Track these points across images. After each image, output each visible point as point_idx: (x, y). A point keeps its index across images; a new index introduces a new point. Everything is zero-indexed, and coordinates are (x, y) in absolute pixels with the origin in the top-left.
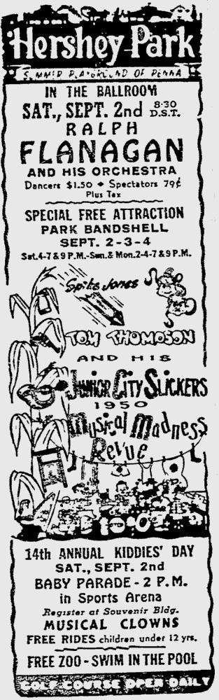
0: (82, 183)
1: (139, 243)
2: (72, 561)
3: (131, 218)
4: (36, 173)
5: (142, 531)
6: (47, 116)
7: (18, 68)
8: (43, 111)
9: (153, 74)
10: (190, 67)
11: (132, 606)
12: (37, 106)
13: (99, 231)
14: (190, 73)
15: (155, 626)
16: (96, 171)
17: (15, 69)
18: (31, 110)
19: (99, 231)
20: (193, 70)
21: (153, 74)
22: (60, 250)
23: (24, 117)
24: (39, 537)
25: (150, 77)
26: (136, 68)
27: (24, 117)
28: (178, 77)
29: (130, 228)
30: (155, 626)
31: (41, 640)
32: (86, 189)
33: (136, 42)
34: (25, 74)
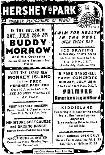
0: (23, 60)
1: (13, 153)
2: (35, 95)
3: (72, 90)
4: (44, 77)
5: (56, 6)
6: (14, 37)
7: (6, 19)
8: (13, 36)
9: (59, 21)
10: (74, 18)
11: (36, 108)
12: (11, 34)
13: (43, 77)
14: (74, 20)
15: (47, 52)
16: (48, 85)
17: (5, 19)
18: (10, 35)
19: (43, 77)
20: (75, 19)
21: (59, 21)
22: (18, 84)
23: (8, 37)
24: (79, 11)
25: (58, 22)
26: (52, 19)
27: (8, 37)
28: (69, 22)
29: (20, 85)
30: (47, 52)
31: (23, 122)
32: (24, 62)
33: (54, 10)
34: (9, 21)
